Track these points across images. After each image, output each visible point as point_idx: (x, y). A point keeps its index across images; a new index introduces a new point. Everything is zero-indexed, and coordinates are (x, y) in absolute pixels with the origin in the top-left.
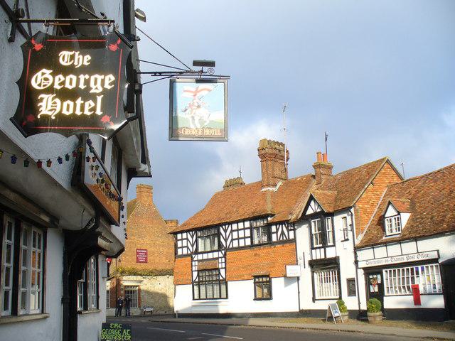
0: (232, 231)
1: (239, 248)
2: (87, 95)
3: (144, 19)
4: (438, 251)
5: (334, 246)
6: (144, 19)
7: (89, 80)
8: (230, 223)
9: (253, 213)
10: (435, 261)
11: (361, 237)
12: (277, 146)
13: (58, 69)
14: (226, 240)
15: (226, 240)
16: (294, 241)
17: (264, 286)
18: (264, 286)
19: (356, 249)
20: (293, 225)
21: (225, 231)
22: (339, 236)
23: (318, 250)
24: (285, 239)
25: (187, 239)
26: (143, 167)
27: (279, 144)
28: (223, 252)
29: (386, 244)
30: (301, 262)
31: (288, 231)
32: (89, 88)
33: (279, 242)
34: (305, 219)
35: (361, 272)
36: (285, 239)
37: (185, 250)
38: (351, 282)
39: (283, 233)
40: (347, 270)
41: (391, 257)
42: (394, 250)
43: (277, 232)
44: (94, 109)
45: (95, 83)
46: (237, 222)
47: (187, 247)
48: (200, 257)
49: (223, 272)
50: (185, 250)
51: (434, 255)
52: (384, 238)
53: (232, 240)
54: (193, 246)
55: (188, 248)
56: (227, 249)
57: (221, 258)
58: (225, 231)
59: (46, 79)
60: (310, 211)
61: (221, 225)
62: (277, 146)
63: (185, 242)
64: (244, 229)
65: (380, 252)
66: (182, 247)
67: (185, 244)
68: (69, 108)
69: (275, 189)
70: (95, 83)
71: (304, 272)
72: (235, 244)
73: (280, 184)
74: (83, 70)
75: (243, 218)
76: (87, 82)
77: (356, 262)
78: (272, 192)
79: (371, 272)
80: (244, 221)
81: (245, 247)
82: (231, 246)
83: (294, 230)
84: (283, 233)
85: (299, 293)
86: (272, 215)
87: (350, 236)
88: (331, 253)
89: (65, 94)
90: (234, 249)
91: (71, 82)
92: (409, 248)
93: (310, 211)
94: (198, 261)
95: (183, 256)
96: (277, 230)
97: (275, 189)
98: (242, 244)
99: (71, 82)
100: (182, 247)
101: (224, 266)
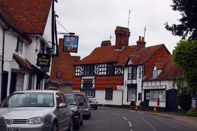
0: (99, 68)
1: (101, 75)
2: (45, 62)
3: (58, 17)
4: (166, 86)
5: (136, 79)
6: (58, 17)
8: (99, 64)
9: (108, 61)
10: (164, 89)
11: (145, 77)
12: (124, 30)
13: (42, 58)
14: (96, 71)
15: (96, 71)
16: (123, 75)
17: (109, 97)
18: (109, 97)
19: (143, 82)
20: (123, 68)
21: (97, 67)
22: (138, 75)
23: (130, 80)
24: (80, 75)
25: (80, 69)
26: (43, 82)
27: (127, 28)
28: (95, 76)
29: (152, 81)
30: (124, 84)
31: (121, 70)
33: (117, 74)
34: (127, 66)
35: (143, 91)
36: (80, 75)
37: (79, 74)
38: (140, 94)
39: (119, 71)
40: (139, 90)
41: (157, 86)
42: (154, 84)
43: (117, 70)
46: (102, 64)
47: (80, 72)
48: (85, 78)
49: (94, 85)
50: (79, 74)
51: (164, 87)
52: (152, 78)
53: (99, 71)
54: (82, 72)
55: (80, 73)
56: (96, 75)
57: (94, 79)
58: (97, 67)
60: (129, 64)
61: (94, 64)
62: (124, 30)
63: (79, 70)
64: (104, 67)
65: (150, 84)
66: (78, 72)
67: (79, 71)
68: (43, 63)
69: (121, 50)
71: (125, 89)
72: (100, 73)
73: (123, 48)
74: (45, 59)
75: (104, 62)
77: (142, 87)
78: (120, 51)
79: (146, 91)
80: (104, 63)
81: (104, 75)
82: (98, 74)
83: (124, 70)
84: (119, 71)
85: (123, 97)
86: (116, 63)
87: (141, 76)
88: (134, 82)
89: (43, 62)
90: (99, 75)
91: (44, 60)
92: (158, 83)
93: (129, 64)
94: (84, 79)
95: (78, 76)
96: (117, 69)
97: (121, 50)
98: (103, 74)
99: (44, 60)
100: (78, 72)
101: (94, 83)
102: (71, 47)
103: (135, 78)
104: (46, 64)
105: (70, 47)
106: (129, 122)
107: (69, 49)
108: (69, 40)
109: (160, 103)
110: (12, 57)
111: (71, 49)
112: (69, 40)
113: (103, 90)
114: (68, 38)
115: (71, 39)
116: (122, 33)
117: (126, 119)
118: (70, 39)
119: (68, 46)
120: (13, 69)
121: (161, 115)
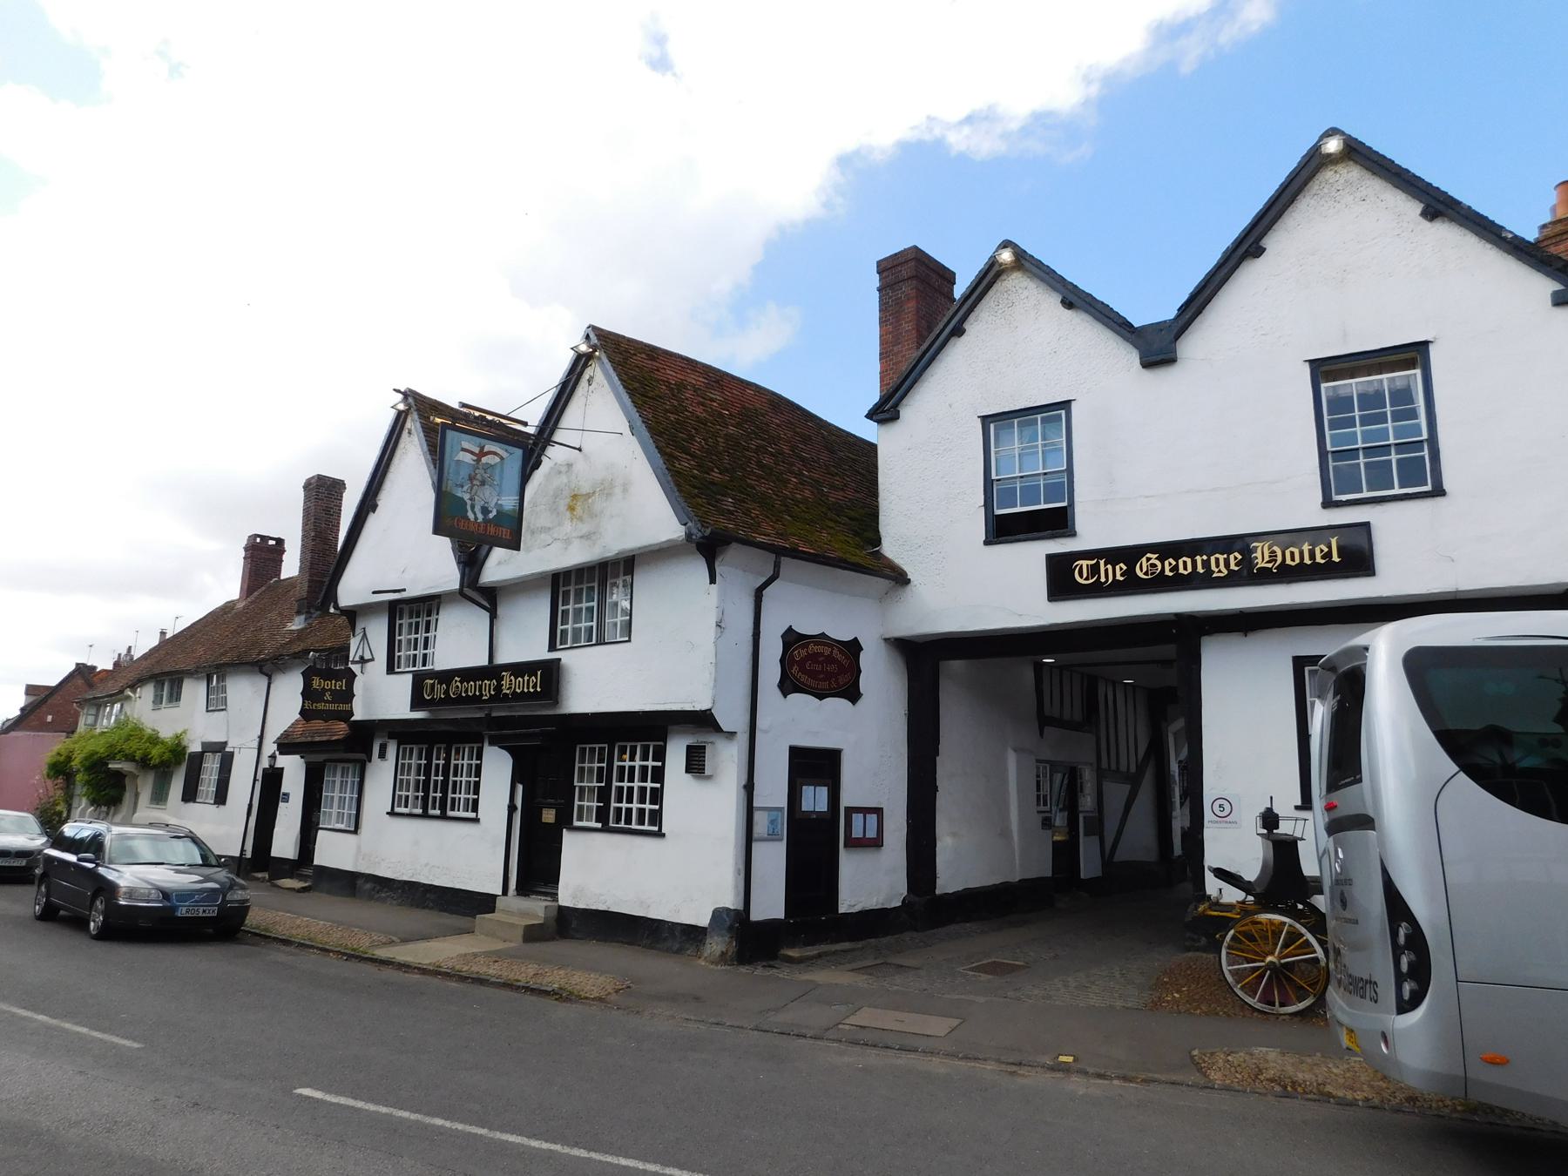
7: (1209, 561)
32: (1209, 571)
44: (1328, 555)
45: (1218, 565)
59: (1153, 565)
70: (1218, 565)
76: (1206, 564)
102: (485, 511)
103: (437, 812)
104: (535, 686)
105: (478, 509)
106: (299, 1091)
107: (471, 516)
108: (468, 458)
109: (320, 832)
110: (191, 805)
111: (486, 521)
112: (468, 458)
113: (323, 870)
114: (466, 445)
115: (482, 454)
116: (163, 633)
117: (306, 1092)
118: (477, 450)
119: (466, 497)
120: (1438, 491)
121: (335, 938)
